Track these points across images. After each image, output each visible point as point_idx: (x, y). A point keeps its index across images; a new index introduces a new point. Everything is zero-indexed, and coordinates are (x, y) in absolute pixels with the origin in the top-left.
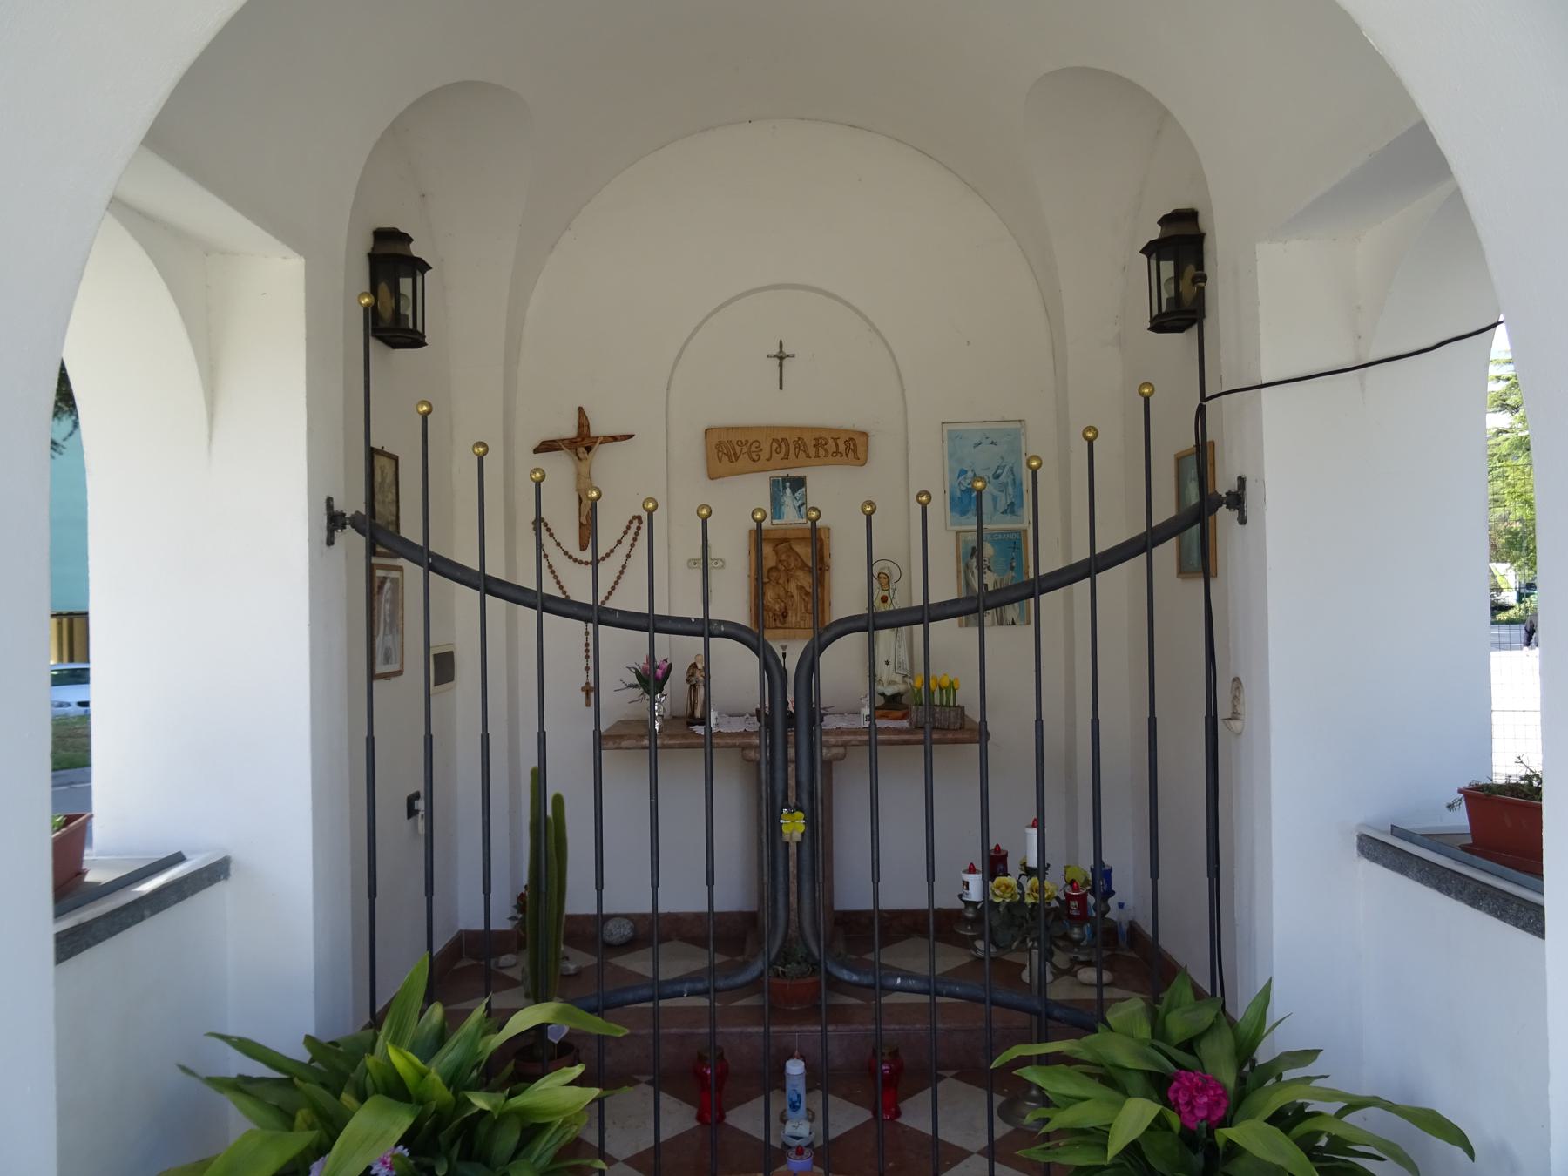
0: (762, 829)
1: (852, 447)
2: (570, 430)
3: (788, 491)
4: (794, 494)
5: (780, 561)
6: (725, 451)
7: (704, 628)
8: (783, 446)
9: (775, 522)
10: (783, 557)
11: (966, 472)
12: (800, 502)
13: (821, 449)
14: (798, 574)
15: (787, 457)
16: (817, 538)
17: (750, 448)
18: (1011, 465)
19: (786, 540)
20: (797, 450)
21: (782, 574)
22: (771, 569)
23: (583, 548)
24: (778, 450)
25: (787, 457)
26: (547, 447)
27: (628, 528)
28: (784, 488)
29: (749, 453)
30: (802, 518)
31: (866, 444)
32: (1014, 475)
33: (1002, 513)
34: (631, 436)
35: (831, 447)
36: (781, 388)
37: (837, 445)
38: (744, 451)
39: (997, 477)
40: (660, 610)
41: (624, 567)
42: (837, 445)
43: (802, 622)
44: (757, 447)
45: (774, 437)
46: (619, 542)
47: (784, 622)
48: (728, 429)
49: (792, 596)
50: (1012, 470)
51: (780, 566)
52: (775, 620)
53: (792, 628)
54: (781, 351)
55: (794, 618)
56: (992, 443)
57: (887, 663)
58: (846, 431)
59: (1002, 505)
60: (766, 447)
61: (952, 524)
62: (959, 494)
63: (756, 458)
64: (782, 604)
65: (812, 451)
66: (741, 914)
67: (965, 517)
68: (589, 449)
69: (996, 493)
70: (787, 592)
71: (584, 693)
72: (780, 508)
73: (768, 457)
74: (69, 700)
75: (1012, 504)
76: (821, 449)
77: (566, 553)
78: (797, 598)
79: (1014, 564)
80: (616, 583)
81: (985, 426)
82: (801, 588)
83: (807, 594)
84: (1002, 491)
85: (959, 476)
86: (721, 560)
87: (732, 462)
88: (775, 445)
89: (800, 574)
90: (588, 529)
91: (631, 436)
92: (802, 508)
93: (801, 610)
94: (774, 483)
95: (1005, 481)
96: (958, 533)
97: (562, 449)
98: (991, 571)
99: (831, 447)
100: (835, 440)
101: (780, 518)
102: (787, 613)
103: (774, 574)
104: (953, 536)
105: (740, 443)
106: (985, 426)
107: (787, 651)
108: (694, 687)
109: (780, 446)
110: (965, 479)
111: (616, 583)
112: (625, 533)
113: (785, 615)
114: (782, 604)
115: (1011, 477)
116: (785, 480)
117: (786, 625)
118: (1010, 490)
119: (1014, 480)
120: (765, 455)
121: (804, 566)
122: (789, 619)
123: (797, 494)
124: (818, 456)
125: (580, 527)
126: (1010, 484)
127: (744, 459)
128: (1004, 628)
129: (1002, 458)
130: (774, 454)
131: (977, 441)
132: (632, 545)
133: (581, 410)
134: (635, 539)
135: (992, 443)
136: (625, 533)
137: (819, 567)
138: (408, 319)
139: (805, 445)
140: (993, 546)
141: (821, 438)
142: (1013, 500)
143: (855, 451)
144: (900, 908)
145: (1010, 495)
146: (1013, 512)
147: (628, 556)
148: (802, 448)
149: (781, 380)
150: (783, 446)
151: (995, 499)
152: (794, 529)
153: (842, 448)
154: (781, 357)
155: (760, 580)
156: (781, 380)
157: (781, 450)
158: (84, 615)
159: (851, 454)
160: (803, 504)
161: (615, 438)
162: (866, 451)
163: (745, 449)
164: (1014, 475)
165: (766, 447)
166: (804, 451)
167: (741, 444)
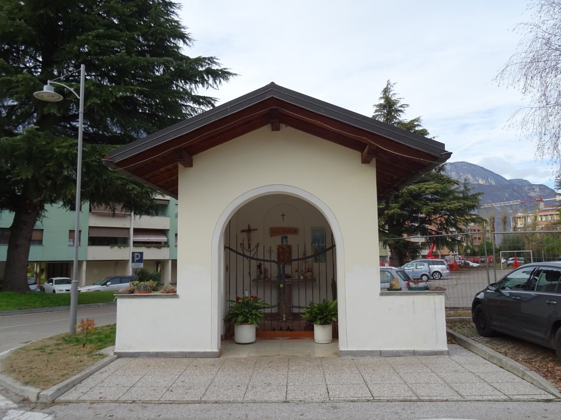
0: (267, 90)
2: (246, 228)
7: (270, 261)
16: (289, 247)
23: (249, 248)
26: (243, 231)
34: (257, 229)
40: (265, 259)
68: (250, 232)
74: (63, 289)
90: (249, 247)
91: (257, 229)
133: (249, 225)
137: (290, 253)
138: (70, 87)
154: (283, 215)
155: (279, 255)
158: (176, 260)
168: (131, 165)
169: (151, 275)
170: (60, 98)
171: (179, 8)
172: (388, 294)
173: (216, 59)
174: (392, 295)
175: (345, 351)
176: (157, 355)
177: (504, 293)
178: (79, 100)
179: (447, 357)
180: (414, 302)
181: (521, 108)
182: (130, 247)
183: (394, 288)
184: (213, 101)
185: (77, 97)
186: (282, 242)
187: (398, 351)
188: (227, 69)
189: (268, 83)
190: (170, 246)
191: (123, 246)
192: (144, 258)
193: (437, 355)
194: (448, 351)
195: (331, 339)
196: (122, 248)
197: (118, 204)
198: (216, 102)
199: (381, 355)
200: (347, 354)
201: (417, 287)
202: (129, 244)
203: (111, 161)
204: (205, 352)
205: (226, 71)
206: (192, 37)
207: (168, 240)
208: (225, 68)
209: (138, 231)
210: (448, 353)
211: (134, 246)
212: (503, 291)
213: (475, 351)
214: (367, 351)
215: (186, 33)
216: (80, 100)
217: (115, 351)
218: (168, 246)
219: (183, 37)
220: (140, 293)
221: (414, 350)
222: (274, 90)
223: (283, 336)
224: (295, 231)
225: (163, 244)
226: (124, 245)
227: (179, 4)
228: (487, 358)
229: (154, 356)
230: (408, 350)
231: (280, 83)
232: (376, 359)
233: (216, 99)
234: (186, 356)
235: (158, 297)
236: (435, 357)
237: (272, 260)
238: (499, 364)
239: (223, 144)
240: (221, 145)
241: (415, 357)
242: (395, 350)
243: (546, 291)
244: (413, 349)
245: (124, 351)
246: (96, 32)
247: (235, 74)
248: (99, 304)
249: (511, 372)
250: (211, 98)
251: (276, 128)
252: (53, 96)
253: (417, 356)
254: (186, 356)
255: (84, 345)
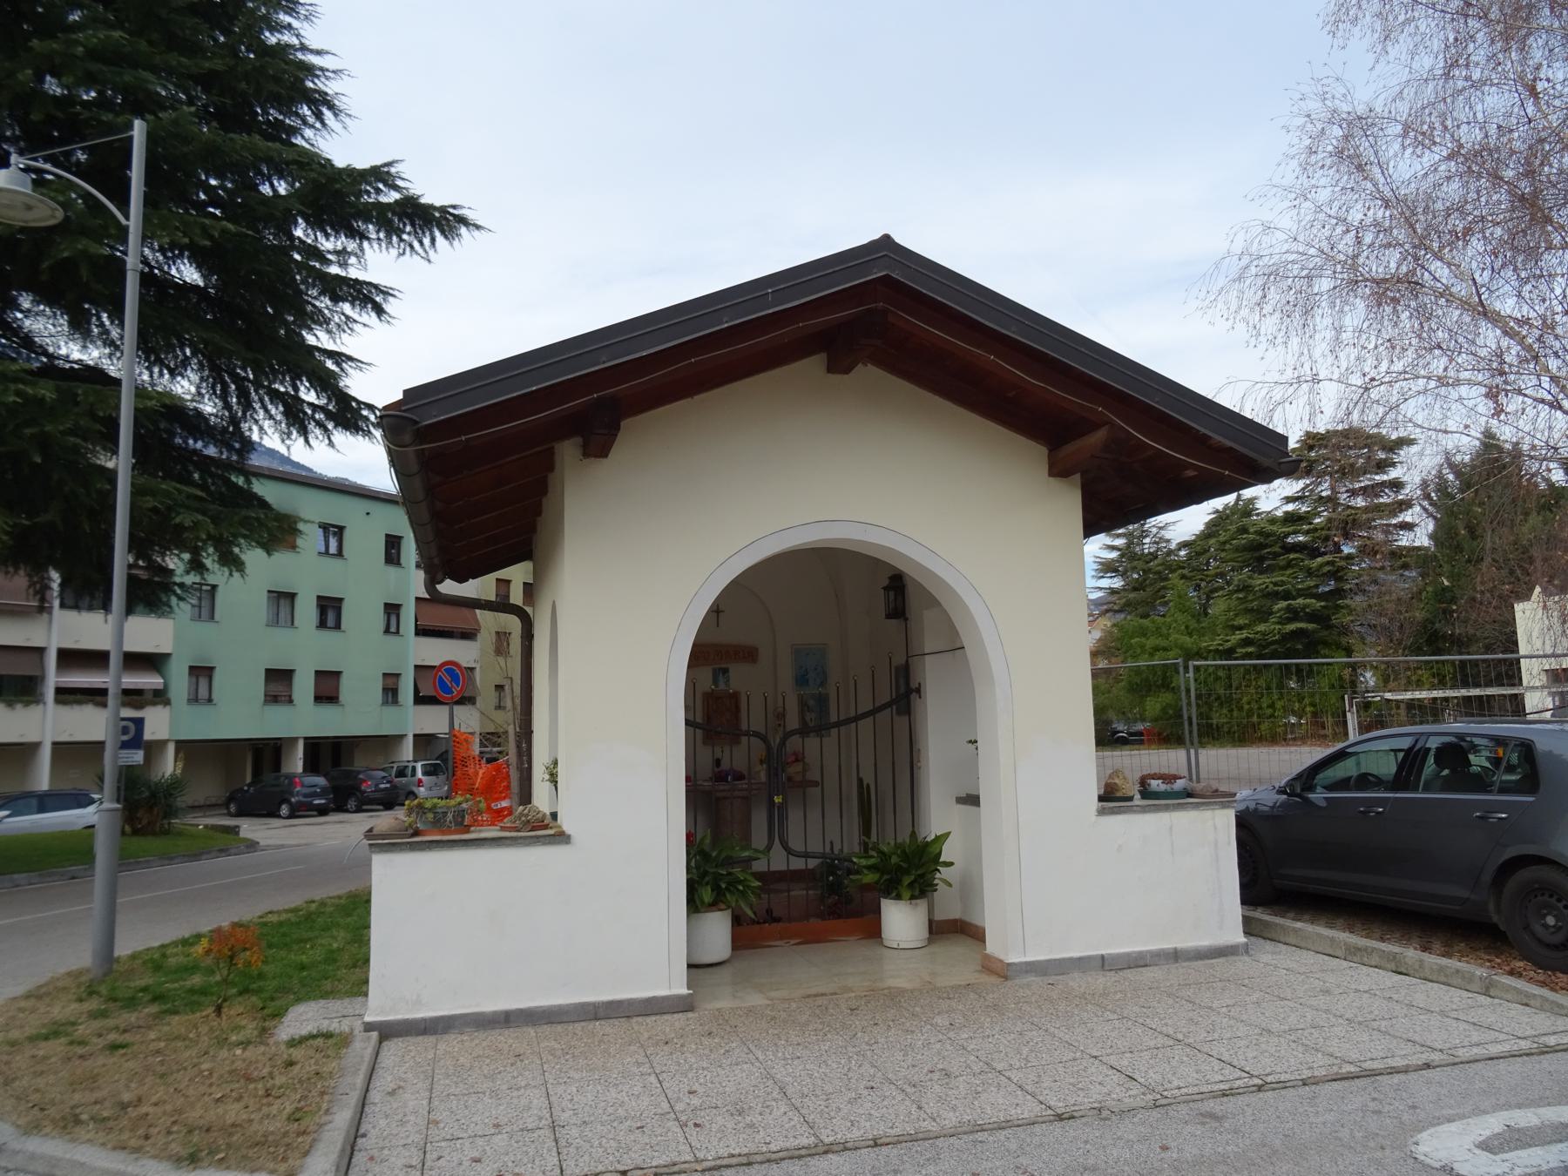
168: (463, 438)
169: (156, 784)
170: (53, 217)
171: (306, 17)
172: (1115, 810)
173: (400, 178)
174: (1125, 812)
175: (1021, 964)
176: (507, 1019)
177: (1313, 800)
178: (125, 230)
179: (1246, 958)
180: (1171, 828)
181: (1230, 380)
182: (45, 703)
183: (1119, 794)
184: (381, 296)
185: (118, 222)
186: (715, 682)
187: (1140, 953)
188: (462, 207)
189: (877, 236)
190: (173, 701)
191: (21, 702)
192: (147, 736)
193: (1224, 956)
194: (1247, 944)
195: (926, 935)
196: (19, 706)
197: (11, 569)
198: (391, 299)
199: (1103, 965)
200: (1027, 972)
201: (1169, 790)
202: (42, 694)
203: (411, 419)
204: (654, 998)
205: (456, 212)
206: (346, 107)
207: (166, 685)
208: (454, 203)
209: (71, 658)
210: (1246, 949)
211: (58, 701)
212: (1310, 796)
213: (1292, 940)
214: (1071, 960)
215: (330, 92)
216: (131, 230)
217: (367, 1019)
218: (167, 702)
219: (320, 102)
220: (443, 833)
221: (1175, 949)
222: (890, 257)
223: (783, 936)
224: (748, 654)
225: (149, 696)
226: (26, 698)
227: (311, 5)
228: (1339, 953)
229: (499, 1022)
230: (1163, 950)
231: (903, 239)
232: (1101, 981)
233: (391, 291)
234: (596, 1013)
235: (508, 842)
236: (1222, 960)
237: (752, 729)
238: (1392, 966)
239: (695, 397)
240: (689, 399)
241: (1177, 965)
242: (1135, 952)
243: (1387, 790)
244: (1174, 946)
245: (399, 1017)
246: (102, 37)
247: (478, 227)
248: (16, 876)
249: (1437, 982)
250: (376, 287)
251: (839, 365)
252: (29, 208)
253: (1185, 961)
254: (596, 1013)
255: (219, 1010)
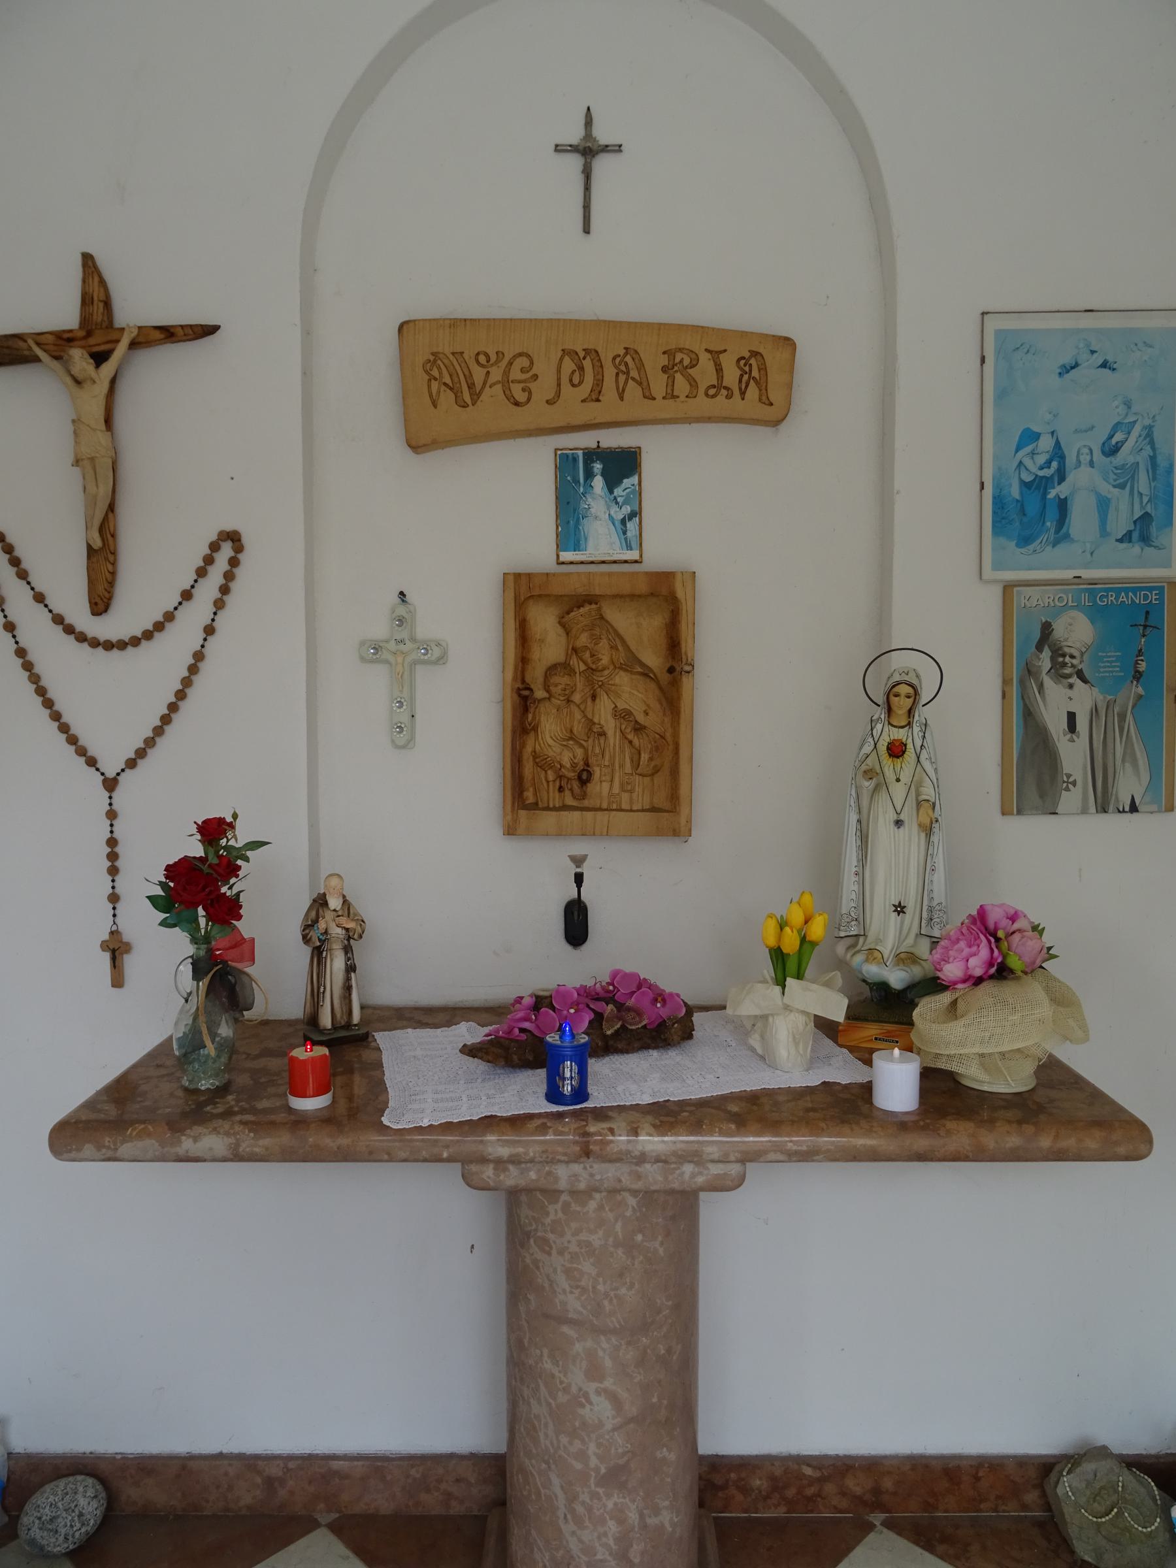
1: (755, 373)
3: (598, 482)
4: (611, 492)
5: (575, 650)
6: (448, 380)
8: (587, 364)
9: (567, 556)
10: (583, 640)
11: (1036, 437)
12: (627, 509)
13: (678, 376)
14: (617, 680)
15: (596, 396)
17: (506, 373)
18: (1147, 422)
19: (590, 599)
20: (622, 378)
21: (580, 682)
22: (552, 669)
24: (576, 380)
25: (596, 396)
27: (209, 560)
28: (589, 475)
29: (506, 383)
30: (629, 548)
31: (790, 367)
32: (1153, 449)
33: (1120, 541)
35: (705, 372)
36: (587, 230)
37: (719, 369)
38: (492, 379)
39: (1112, 450)
41: (199, 656)
42: (719, 369)
43: (625, 797)
44: (522, 370)
45: (569, 346)
46: (187, 595)
47: (584, 796)
48: (456, 324)
49: (603, 734)
50: (1149, 434)
51: (574, 661)
52: (561, 789)
53: (600, 809)
54: (588, 135)
55: (606, 786)
56: (1104, 365)
57: (900, 909)
58: (744, 335)
59: (1121, 522)
60: (545, 368)
61: (997, 566)
62: (1015, 492)
63: (521, 397)
64: (579, 752)
65: (658, 384)
66: (474, 1458)
67: (1023, 550)
69: (1106, 489)
70: (590, 723)
71: (107, 956)
72: (578, 522)
73: (550, 396)
75: (1146, 518)
76: (678, 376)
77: (58, 619)
78: (613, 738)
79: (1143, 666)
80: (181, 695)
81: (1088, 322)
82: (623, 715)
83: (639, 728)
84: (1122, 486)
85: (1017, 451)
86: (438, 645)
87: (465, 406)
88: (569, 365)
89: (622, 680)
92: (629, 525)
93: (622, 766)
94: (565, 462)
95: (1131, 460)
96: (1008, 589)
97: (37, 360)
98: (1085, 681)
99: (705, 372)
100: (715, 354)
101: (577, 547)
102: (590, 774)
103: (561, 680)
104: (993, 597)
105: (482, 359)
106: (1088, 322)
107: (585, 869)
108: (319, 954)
109: (581, 368)
110: (1033, 453)
111: (181, 695)
112: (201, 573)
113: (584, 777)
114: (579, 752)
115: (1148, 450)
116: (591, 455)
117: (586, 803)
118: (1143, 483)
119: (1153, 459)
120: (543, 389)
121: (632, 664)
122: (592, 788)
123: (618, 491)
124: (671, 396)
125: (89, 557)
126: (1142, 467)
127: (493, 396)
128: (1112, 821)
129: (1128, 404)
130: (566, 388)
131: (1067, 360)
132: (219, 605)
133: (88, 260)
134: (225, 590)
135: (1104, 365)
136: (201, 573)
139: (641, 367)
140: (1093, 621)
141: (681, 350)
142: (1148, 509)
143: (763, 386)
144: (841, 1452)
145: (1141, 495)
146: (1145, 539)
147: (209, 630)
148: (634, 373)
149: (587, 207)
150: (587, 364)
151: (1103, 505)
152: (610, 574)
153: (731, 375)
156: (587, 207)
157: (582, 376)
159: (753, 392)
160: (632, 515)
161: (169, 334)
162: (790, 386)
163: (496, 374)
164: (1153, 449)
165: (545, 368)
166: (640, 384)
167: (484, 359)
